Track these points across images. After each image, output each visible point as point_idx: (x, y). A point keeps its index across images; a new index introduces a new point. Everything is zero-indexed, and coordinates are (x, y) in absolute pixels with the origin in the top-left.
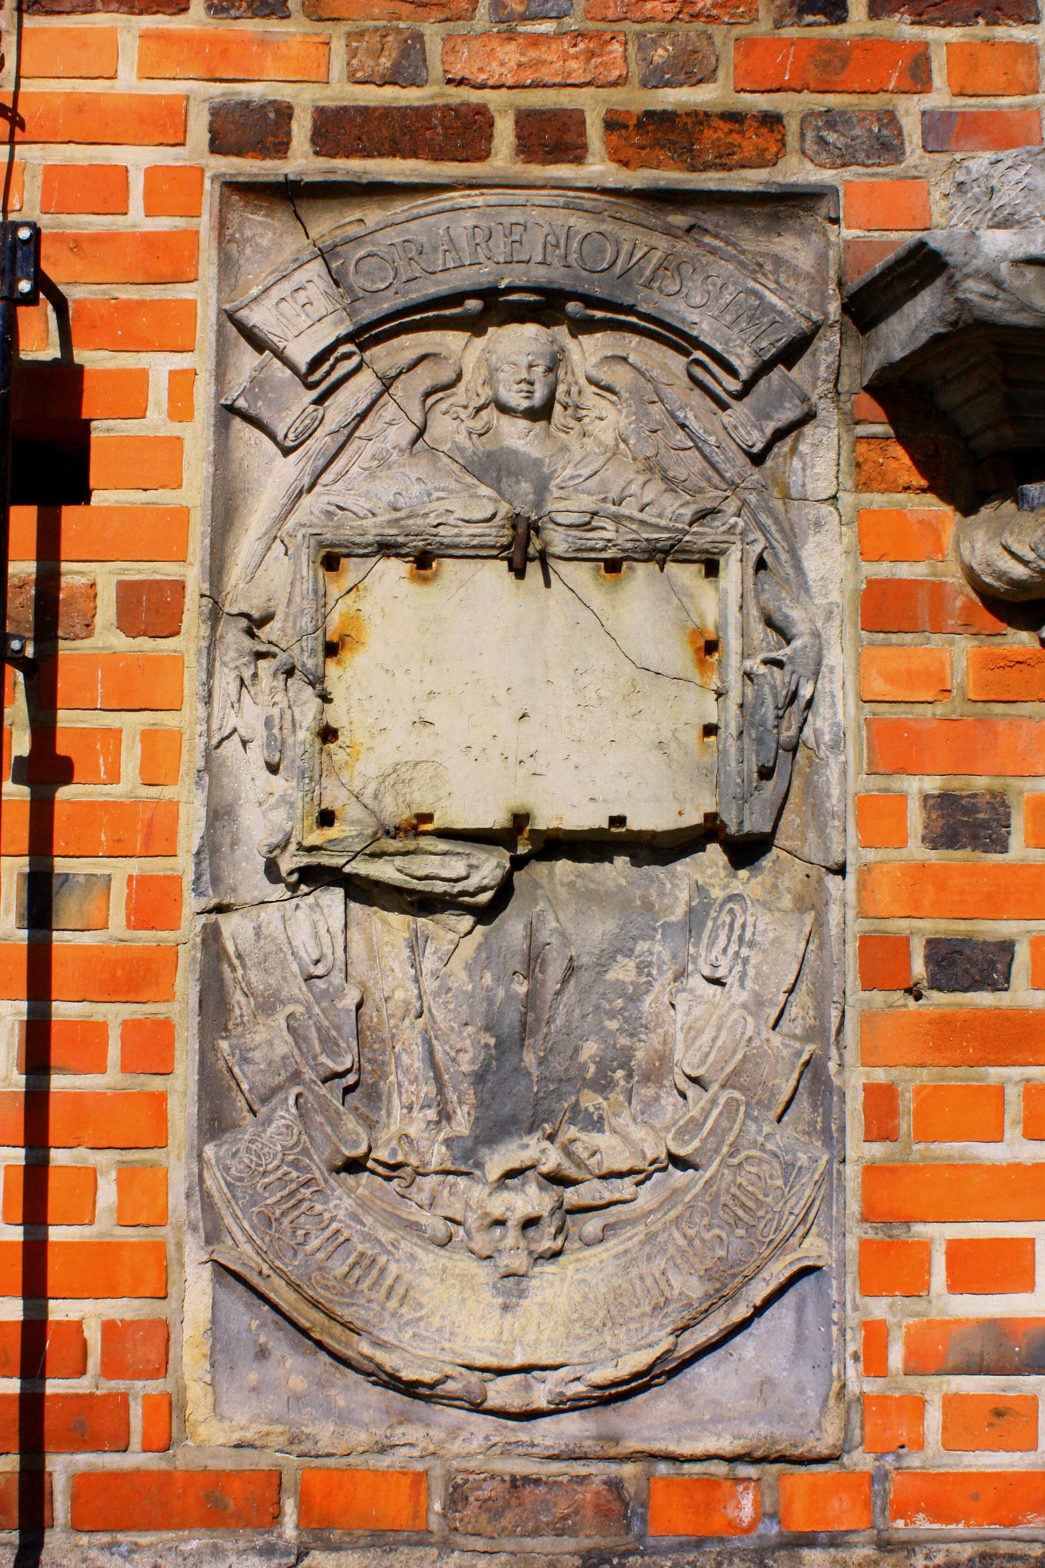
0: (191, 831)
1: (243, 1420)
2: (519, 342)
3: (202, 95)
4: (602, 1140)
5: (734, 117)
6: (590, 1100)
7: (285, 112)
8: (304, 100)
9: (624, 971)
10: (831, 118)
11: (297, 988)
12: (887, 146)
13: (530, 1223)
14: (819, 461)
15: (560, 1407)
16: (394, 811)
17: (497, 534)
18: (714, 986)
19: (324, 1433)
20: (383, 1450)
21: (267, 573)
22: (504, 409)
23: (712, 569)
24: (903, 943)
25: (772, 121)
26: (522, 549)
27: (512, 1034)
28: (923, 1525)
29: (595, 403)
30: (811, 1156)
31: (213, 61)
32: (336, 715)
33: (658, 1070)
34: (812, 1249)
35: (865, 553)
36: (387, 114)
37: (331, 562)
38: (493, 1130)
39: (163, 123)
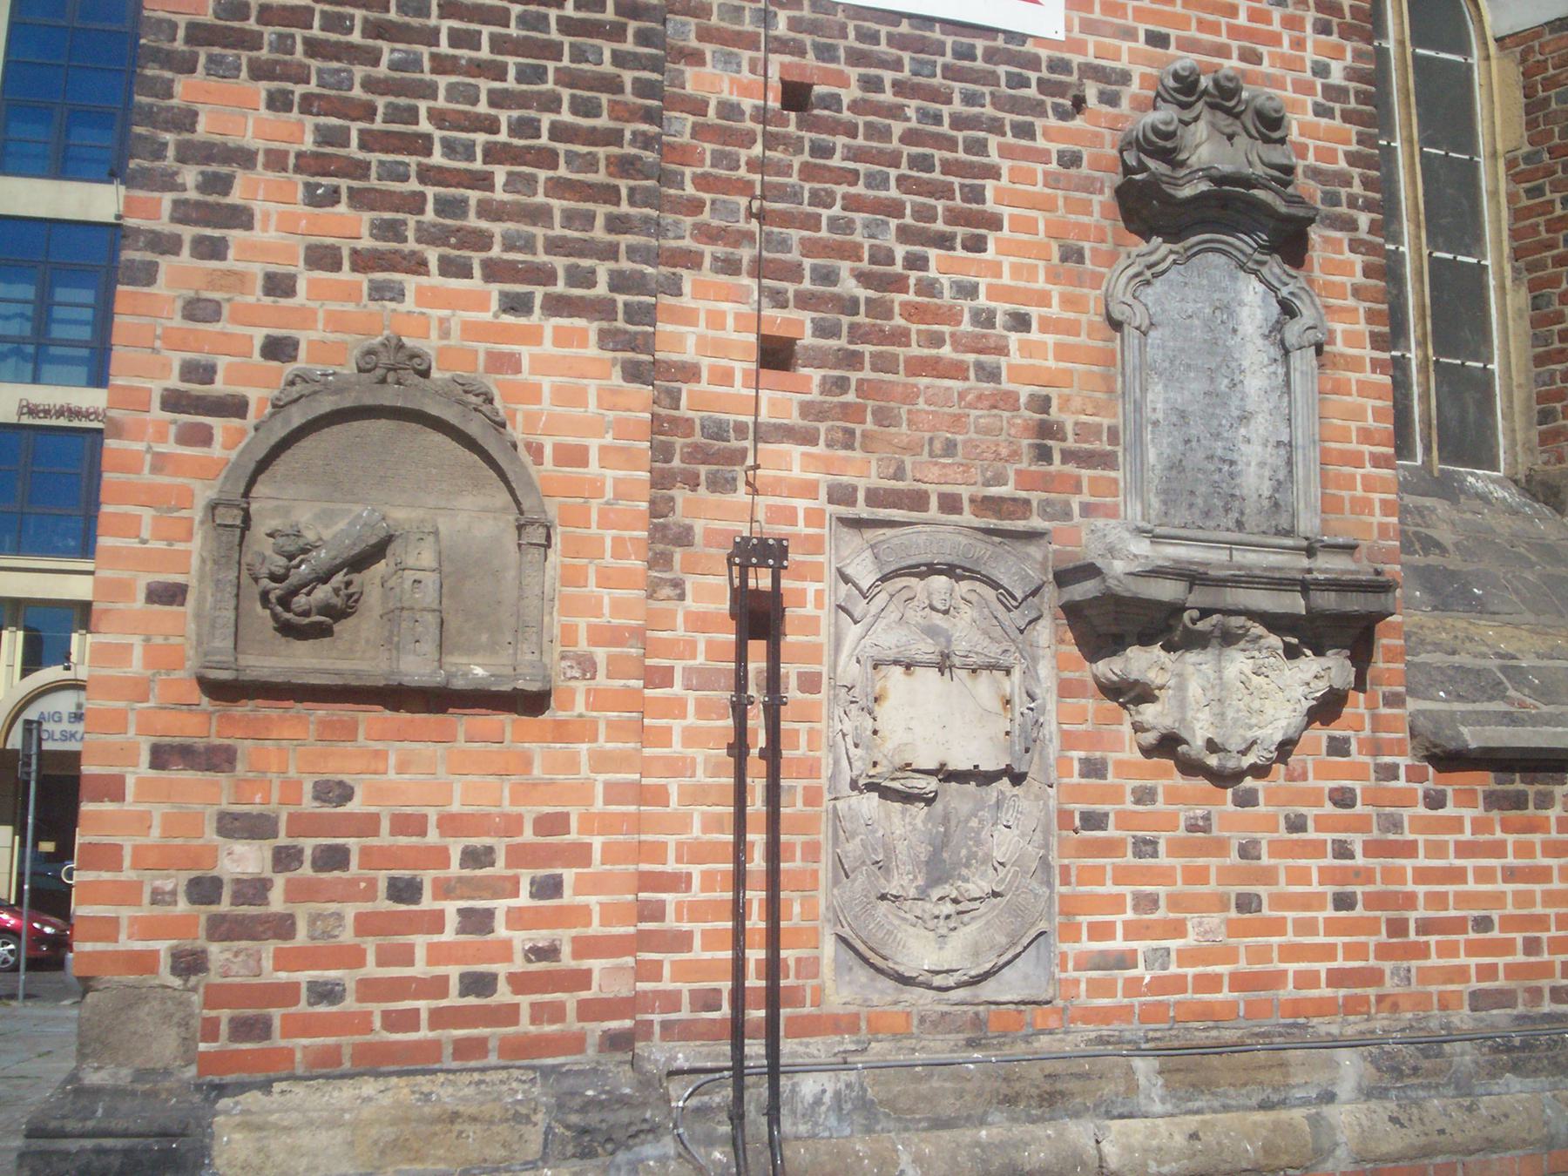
0: (826, 772)
1: (846, 994)
2: (940, 581)
3: (823, 480)
4: (970, 886)
5: (1014, 500)
6: (964, 872)
7: (855, 489)
8: (862, 485)
9: (974, 823)
10: (1048, 502)
11: (863, 829)
12: (1067, 514)
13: (948, 917)
14: (1044, 633)
15: (959, 985)
16: (899, 762)
17: (936, 658)
18: (1011, 831)
19: (875, 998)
20: (896, 1003)
21: (849, 670)
22: (933, 608)
23: (1008, 673)
24: (1072, 813)
25: (1027, 502)
26: (944, 664)
27: (940, 845)
28: (1080, 1026)
29: (964, 607)
30: (1044, 890)
31: (827, 466)
32: (878, 725)
33: (988, 858)
34: (1042, 926)
35: (1060, 668)
36: (893, 492)
37: (875, 667)
38: (935, 880)
39: (809, 490)
